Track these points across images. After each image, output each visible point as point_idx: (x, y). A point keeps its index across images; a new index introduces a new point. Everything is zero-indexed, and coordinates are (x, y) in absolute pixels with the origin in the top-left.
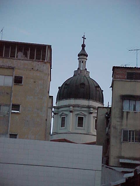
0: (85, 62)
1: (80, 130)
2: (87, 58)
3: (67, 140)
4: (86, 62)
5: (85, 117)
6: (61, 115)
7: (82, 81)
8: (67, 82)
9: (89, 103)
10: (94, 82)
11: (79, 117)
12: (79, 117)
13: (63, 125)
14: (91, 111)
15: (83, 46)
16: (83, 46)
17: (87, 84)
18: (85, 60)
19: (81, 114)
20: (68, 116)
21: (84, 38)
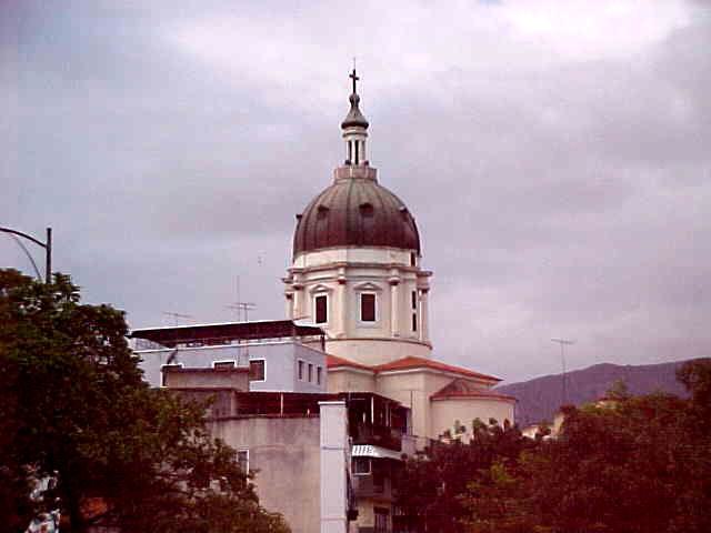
0: (363, 143)
1: (368, 329)
2: (368, 130)
3: (152, 339)
4: (366, 144)
5: (331, 295)
6: (314, 291)
7: (365, 200)
8: (324, 201)
9: (348, 256)
10: (23, 239)
11: (363, 295)
12: (363, 295)
13: (368, 313)
14: (53, 282)
15: (354, 101)
16: (354, 101)
17: (377, 204)
18: (362, 138)
19: (368, 287)
20: (334, 294)
21: (354, 77)
